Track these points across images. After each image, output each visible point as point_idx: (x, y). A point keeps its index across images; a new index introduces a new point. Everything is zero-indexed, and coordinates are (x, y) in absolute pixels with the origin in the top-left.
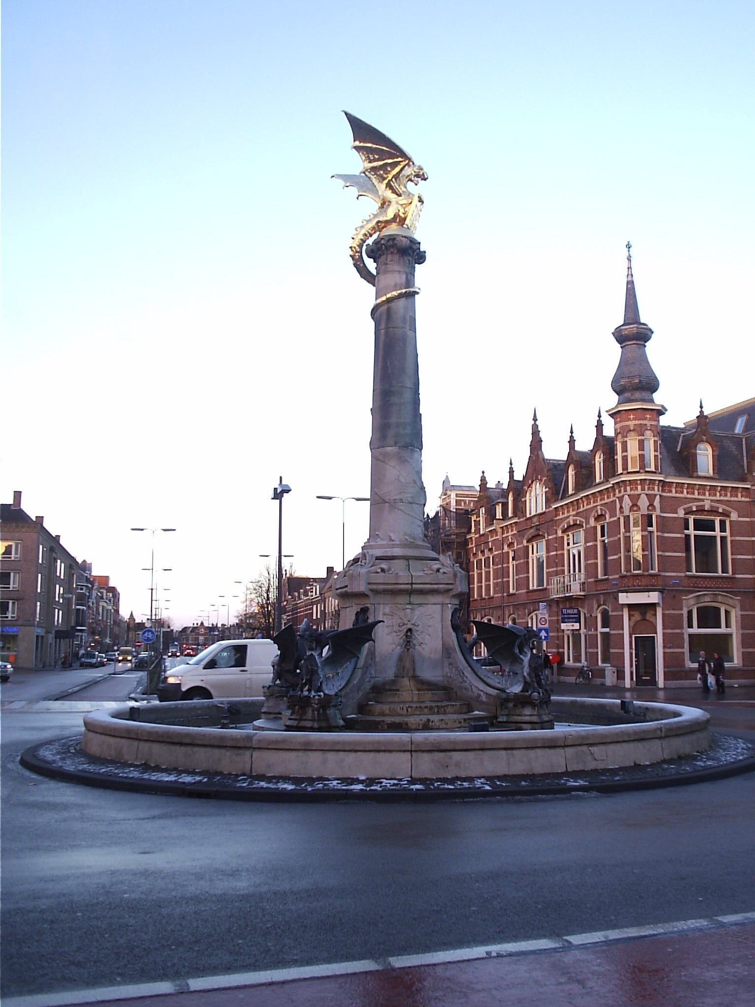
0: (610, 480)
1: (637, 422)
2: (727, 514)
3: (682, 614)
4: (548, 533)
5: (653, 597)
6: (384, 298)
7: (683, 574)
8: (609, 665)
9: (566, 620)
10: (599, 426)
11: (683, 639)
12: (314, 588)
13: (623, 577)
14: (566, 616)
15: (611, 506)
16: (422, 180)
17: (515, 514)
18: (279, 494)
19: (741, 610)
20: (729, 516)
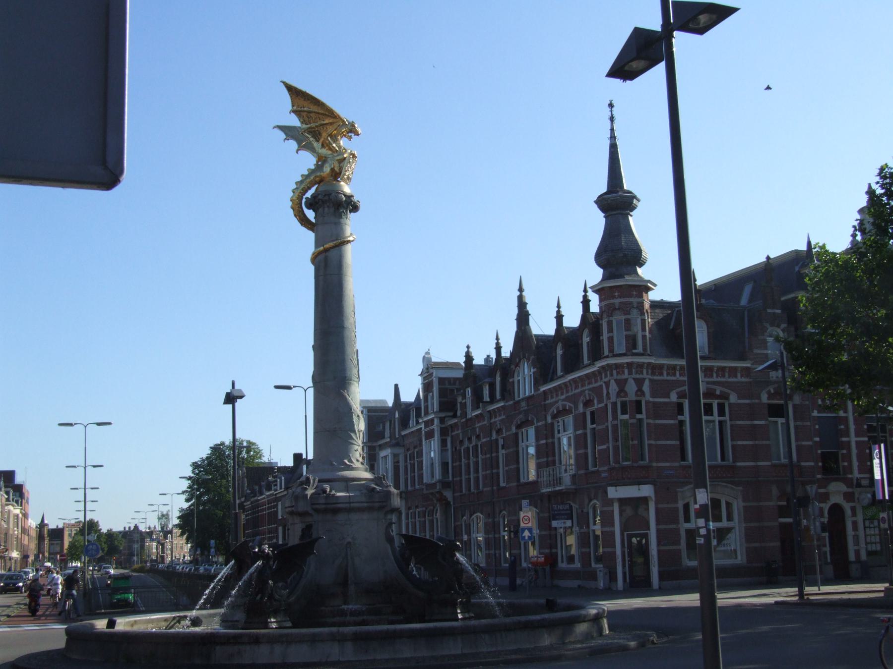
0: (595, 363)
1: (622, 300)
2: (725, 396)
3: (677, 508)
4: (537, 419)
5: (646, 491)
6: (322, 248)
7: (676, 464)
8: (602, 566)
9: (557, 517)
10: (586, 302)
11: (679, 534)
12: (278, 480)
13: (611, 469)
14: (556, 512)
15: (598, 391)
16: (355, 135)
17: (503, 398)
18: (231, 399)
19: (744, 502)
20: (727, 398)
